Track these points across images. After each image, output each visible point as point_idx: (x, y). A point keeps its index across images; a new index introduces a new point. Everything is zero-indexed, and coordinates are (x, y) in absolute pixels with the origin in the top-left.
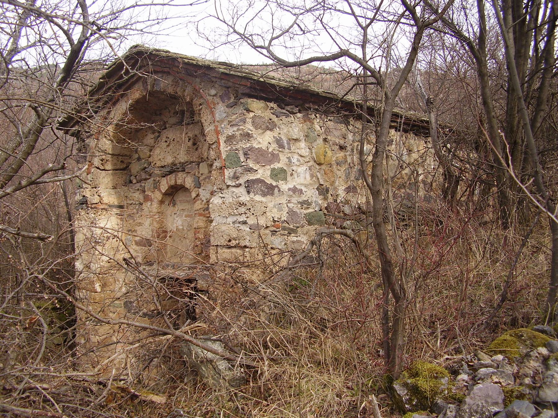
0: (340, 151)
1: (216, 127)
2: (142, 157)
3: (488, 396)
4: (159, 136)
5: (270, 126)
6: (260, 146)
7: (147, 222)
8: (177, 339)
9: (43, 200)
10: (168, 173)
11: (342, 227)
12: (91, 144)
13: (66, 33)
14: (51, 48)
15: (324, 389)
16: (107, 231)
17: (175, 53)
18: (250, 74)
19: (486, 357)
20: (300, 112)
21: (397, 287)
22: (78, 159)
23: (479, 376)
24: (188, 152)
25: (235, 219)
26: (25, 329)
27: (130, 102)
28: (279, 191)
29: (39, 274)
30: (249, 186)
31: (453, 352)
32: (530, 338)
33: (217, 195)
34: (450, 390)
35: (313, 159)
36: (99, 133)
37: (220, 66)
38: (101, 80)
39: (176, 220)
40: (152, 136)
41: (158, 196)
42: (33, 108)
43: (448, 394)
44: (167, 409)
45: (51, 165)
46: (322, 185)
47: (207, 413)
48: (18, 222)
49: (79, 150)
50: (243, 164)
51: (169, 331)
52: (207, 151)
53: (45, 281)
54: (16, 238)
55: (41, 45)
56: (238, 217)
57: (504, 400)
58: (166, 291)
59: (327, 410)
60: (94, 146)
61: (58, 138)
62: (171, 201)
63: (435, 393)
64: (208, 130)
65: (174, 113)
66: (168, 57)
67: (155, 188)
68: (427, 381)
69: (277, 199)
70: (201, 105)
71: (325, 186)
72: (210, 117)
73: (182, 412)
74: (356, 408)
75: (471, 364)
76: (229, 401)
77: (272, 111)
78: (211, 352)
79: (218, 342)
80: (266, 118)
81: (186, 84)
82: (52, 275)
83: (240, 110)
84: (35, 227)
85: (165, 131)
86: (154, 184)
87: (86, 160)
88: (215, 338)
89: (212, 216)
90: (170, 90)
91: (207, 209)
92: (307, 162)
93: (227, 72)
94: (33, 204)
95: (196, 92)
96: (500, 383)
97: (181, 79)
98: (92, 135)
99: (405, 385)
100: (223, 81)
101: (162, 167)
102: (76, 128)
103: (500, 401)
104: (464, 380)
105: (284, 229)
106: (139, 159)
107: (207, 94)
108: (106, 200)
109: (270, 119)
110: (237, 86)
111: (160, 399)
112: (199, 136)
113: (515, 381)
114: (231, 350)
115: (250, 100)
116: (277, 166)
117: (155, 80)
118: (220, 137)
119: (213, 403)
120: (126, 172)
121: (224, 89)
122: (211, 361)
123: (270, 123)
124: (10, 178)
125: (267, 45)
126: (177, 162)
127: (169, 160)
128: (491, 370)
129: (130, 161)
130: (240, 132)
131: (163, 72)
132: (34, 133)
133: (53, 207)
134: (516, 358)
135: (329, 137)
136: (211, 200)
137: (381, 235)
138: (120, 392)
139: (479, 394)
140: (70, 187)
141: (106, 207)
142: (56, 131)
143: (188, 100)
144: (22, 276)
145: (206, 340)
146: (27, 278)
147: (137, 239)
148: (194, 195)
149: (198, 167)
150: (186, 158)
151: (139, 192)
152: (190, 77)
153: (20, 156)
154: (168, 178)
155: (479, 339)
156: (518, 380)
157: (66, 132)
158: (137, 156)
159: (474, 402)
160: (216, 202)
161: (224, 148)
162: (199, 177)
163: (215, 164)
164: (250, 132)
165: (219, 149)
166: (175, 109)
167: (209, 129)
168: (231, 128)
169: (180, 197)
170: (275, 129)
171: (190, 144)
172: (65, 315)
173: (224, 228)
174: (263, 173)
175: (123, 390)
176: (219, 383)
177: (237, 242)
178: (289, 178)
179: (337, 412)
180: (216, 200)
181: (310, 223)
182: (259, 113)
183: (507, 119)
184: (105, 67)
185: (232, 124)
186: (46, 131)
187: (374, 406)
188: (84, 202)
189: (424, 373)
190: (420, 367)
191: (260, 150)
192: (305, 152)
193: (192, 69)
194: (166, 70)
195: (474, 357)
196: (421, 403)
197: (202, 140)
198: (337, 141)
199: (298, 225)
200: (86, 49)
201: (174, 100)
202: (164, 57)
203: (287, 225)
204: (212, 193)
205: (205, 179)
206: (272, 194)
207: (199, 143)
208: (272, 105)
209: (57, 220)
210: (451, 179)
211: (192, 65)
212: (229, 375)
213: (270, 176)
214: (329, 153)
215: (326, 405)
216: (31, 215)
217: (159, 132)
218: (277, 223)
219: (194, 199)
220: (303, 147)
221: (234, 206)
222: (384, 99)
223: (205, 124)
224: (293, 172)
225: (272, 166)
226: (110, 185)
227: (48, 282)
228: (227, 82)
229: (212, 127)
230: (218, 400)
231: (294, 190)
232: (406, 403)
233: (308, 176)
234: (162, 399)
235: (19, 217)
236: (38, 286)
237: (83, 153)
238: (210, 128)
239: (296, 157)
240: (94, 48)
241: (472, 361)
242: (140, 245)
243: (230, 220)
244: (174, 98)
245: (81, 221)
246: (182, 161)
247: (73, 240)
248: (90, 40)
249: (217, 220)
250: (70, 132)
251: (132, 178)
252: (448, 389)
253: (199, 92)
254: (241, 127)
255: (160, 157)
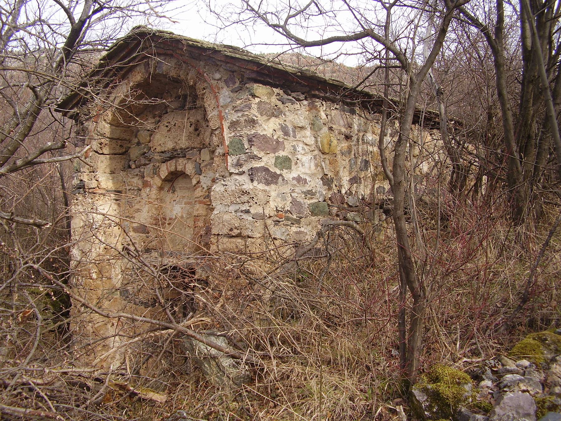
0: (345, 141)
1: (220, 112)
2: (141, 141)
3: (519, 406)
4: (159, 121)
5: (275, 113)
6: (265, 133)
7: (145, 209)
8: (180, 334)
9: (40, 183)
10: (168, 159)
11: (345, 219)
12: (90, 127)
13: (67, 11)
14: (51, 28)
15: (336, 392)
16: (102, 216)
17: (179, 35)
18: (256, 58)
19: (510, 362)
20: (306, 99)
21: (416, 285)
22: (76, 142)
23: (505, 382)
24: (189, 137)
25: (237, 207)
26: (19, 324)
27: (131, 84)
28: (283, 180)
29: (34, 263)
30: (252, 174)
31: (470, 354)
32: (554, 343)
33: (219, 183)
34: (474, 397)
35: (317, 147)
36: (98, 116)
37: (226, 49)
38: (102, 62)
39: (176, 207)
40: (153, 121)
41: (157, 182)
42: (31, 88)
43: (472, 402)
44: (167, 408)
45: (49, 144)
46: (327, 175)
47: (210, 414)
48: (12, 205)
49: (78, 133)
50: (247, 151)
51: (171, 325)
52: (209, 136)
53: (40, 270)
54: (10, 224)
55: (41, 24)
56: (240, 206)
57: (536, 412)
58: (168, 283)
59: (340, 415)
60: (93, 130)
61: (56, 120)
62: (170, 188)
63: (458, 400)
64: (211, 115)
65: (176, 98)
66: (172, 38)
67: (154, 173)
68: (449, 387)
69: (281, 188)
70: (204, 89)
71: (329, 176)
72: (213, 102)
73: (185, 414)
74: (370, 413)
75: (495, 369)
76: (233, 401)
77: (277, 97)
78: (215, 348)
79: (221, 338)
80: (272, 104)
81: (189, 68)
82: (48, 265)
83: (245, 95)
84: (30, 210)
85: (166, 115)
86: (154, 170)
87: (84, 143)
88: (219, 333)
89: (214, 204)
90: (173, 73)
91: (208, 196)
92: (312, 151)
93: (233, 55)
94: (29, 187)
95: (200, 76)
96: (528, 391)
97: (184, 62)
98: (91, 118)
99: (425, 390)
100: (228, 65)
101: (162, 152)
102: (75, 110)
103: (532, 412)
104: (487, 387)
105: (288, 219)
106: (139, 144)
107: (211, 78)
108: (103, 185)
109: (276, 106)
110: (243, 70)
111: (160, 398)
112: (201, 121)
113: (543, 389)
114: (235, 346)
115: (255, 86)
116: (281, 153)
117: (158, 62)
118: (223, 123)
119: (216, 403)
120: (124, 156)
121: (229, 73)
122: (214, 358)
123: (275, 109)
124: (6, 160)
125: (282, 23)
126: (177, 147)
127: (170, 145)
128: (518, 377)
129: (129, 145)
130: (245, 118)
131: (165, 55)
132: (32, 114)
133: (49, 190)
134: (542, 364)
135: (334, 126)
136: (213, 188)
137: (401, 229)
138: (118, 389)
139: (510, 404)
140: (67, 171)
141: (104, 192)
142: (55, 114)
143: (192, 83)
144: (15, 265)
145: (209, 335)
146: (21, 269)
147: (135, 225)
148: (194, 182)
149: (200, 153)
150: (187, 144)
151: (137, 178)
152: (193, 60)
153: (16, 137)
154: (168, 164)
155: (496, 341)
156: (547, 389)
157: (65, 114)
158: (136, 140)
159: (504, 413)
160: (217, 189)
161: (227, 135)
162: (200, 164)
163: (217, 151)
164: (255, 118)
165: (222, 135)
166: (177, 92)
167: (212, 114)
168: (235, 114)
169: (180, 183)
170: (280, 116)
171: (192, 129)
172: (62, 304)
173: (226, 217)
174: (267, 160)
175: (122, 387)
176: (223, 381)
177: (239, 231)
178: (293, 167)
179: (350, 417)
180: (218, 188)
181: (313, 213)
182: (265, 99)
183: (522, 112)
184: (106, 48)
185: (236, 109)
186: (44, 112)
187: (402, 418)
188: (81, 187)
189: (445, 378)
190: (441, 372)
191: (264, 136)
192: (311, 140)
193: (197, 52)
194: (169, 52)
195: (497, 362)
196: (442, 410)
197: (205, 126)
198: (343, 130)
199: (301, 215)
200: (87, 28)
201: (176, 84)
202: (167, 39)
203: (290, 215)
204: (214, 181)
205: (206, 166)
206: (276, 183)
207: (201, 129)
208: (276, 90)
209: (54, 205)
210: (460, 174)
211: (197, 47)
212: (233, 372)
213: (275, 164)
214: (335, 142)
215: (338, 409)
216: (27, 199)
217: (160, 117)
218: (280, 213)
219: (195, 186)
220: (308, 135)
221: (236, 194)
222: (408, 84)
223: (209, 109)
224: (298, 161)
225: (277, 154)
226: (108, 170)
227: (44, 272)
228: (232, 66)
229: (216, 113)
230: (221, 399)
231: (299, 179)
232: (426, 410)
233: (313, 167)
234: (162, 397)
235: (14, 200)
236: (33, 277)
237: (81, 136)
238: (214, 113)
239: (301, 145)
240: (95, 28)
241: (495, 367)
242: (138, 232)
243: (232, 208)
244: (177, 82)
245: (78, 206)
246: (183, 147)
247: (69, 226)
248: (92, 20)
249: (218, 209)
250: (69, 114)
251: (131, 163)
252: (472, 396)
253: (203, 75)
254: (246, 113)
255: (160, 142)
